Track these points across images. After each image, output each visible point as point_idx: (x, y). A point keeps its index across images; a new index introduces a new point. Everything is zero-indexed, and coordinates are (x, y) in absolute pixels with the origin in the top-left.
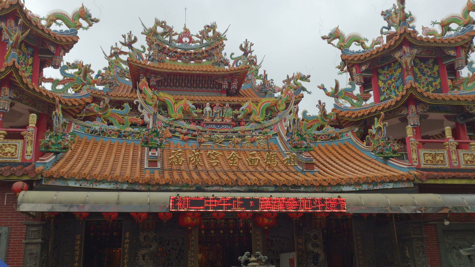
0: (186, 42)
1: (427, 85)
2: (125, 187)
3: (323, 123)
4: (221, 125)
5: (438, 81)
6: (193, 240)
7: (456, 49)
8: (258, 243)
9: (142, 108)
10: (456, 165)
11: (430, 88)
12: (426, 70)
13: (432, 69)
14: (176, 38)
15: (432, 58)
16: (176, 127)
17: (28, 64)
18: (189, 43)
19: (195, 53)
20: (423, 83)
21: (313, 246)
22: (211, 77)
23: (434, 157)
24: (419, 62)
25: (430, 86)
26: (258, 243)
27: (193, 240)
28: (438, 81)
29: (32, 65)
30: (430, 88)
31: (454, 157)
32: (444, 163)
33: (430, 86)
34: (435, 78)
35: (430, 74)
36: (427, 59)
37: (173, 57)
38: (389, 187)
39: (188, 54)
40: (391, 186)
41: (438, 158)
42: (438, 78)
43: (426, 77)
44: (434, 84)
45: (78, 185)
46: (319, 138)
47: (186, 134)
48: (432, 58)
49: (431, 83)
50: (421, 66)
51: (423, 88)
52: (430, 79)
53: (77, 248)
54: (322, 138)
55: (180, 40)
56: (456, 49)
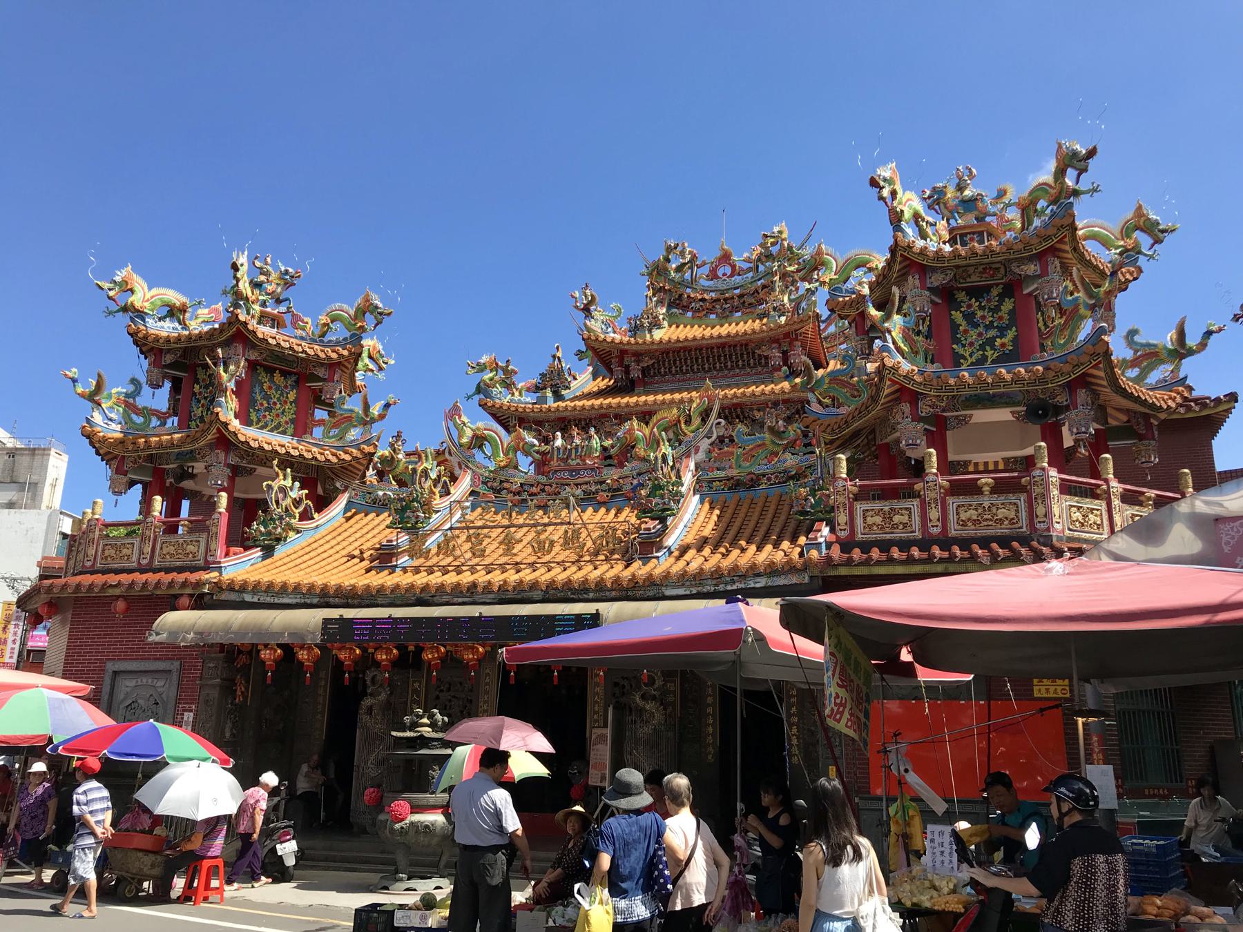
0: (724, 275)
1: (982, 347)
2: (315, 601)
3: (776, 449)
4: (577, 471)
5: (1011, 334)
6: (488, 684)
7: (1041, 257)
8: (598, 689)
9: (450, 454)
10: (935, 531)
11: (989, 353)
12: (980, 313)
13: (997, 309)
14: (706, 270)
15: (997, 285)
16: (502, 482)
17: (286, 402)
18: (732, 276)
19: (741, 296)
20: (971, 344)
21: (643, 697)
22: (747, 345)
23: (888, 517)
24: (966, 299)
25: (988, 348)
26: (598, 689)
27: (488, 684)
28: (1011, 334)
29: (296, 401)
30: (989, 353)
31: (934, 514)
32: (909, 529)
33: (988, 348)
34: (1002, 331)
35: (992, 322)
36: (987, 289)
37: (698, 311)
38: (758, 585)
39: (726, 300)
40: (761, 583)
41: (897, 519)
42: (1008, 327)
43: (981, 329)
44: (998, 342)
45: (255, 600)
46: (764, 480)
47: (519, 493)
48: (997, 285)
49: (991, 342)
50: (969, 306)
51: (971, 356)
52: (992, 333)
53: (321, 691)
54: (769, 479)
55: (713, 275)
56: (1041, 257)
